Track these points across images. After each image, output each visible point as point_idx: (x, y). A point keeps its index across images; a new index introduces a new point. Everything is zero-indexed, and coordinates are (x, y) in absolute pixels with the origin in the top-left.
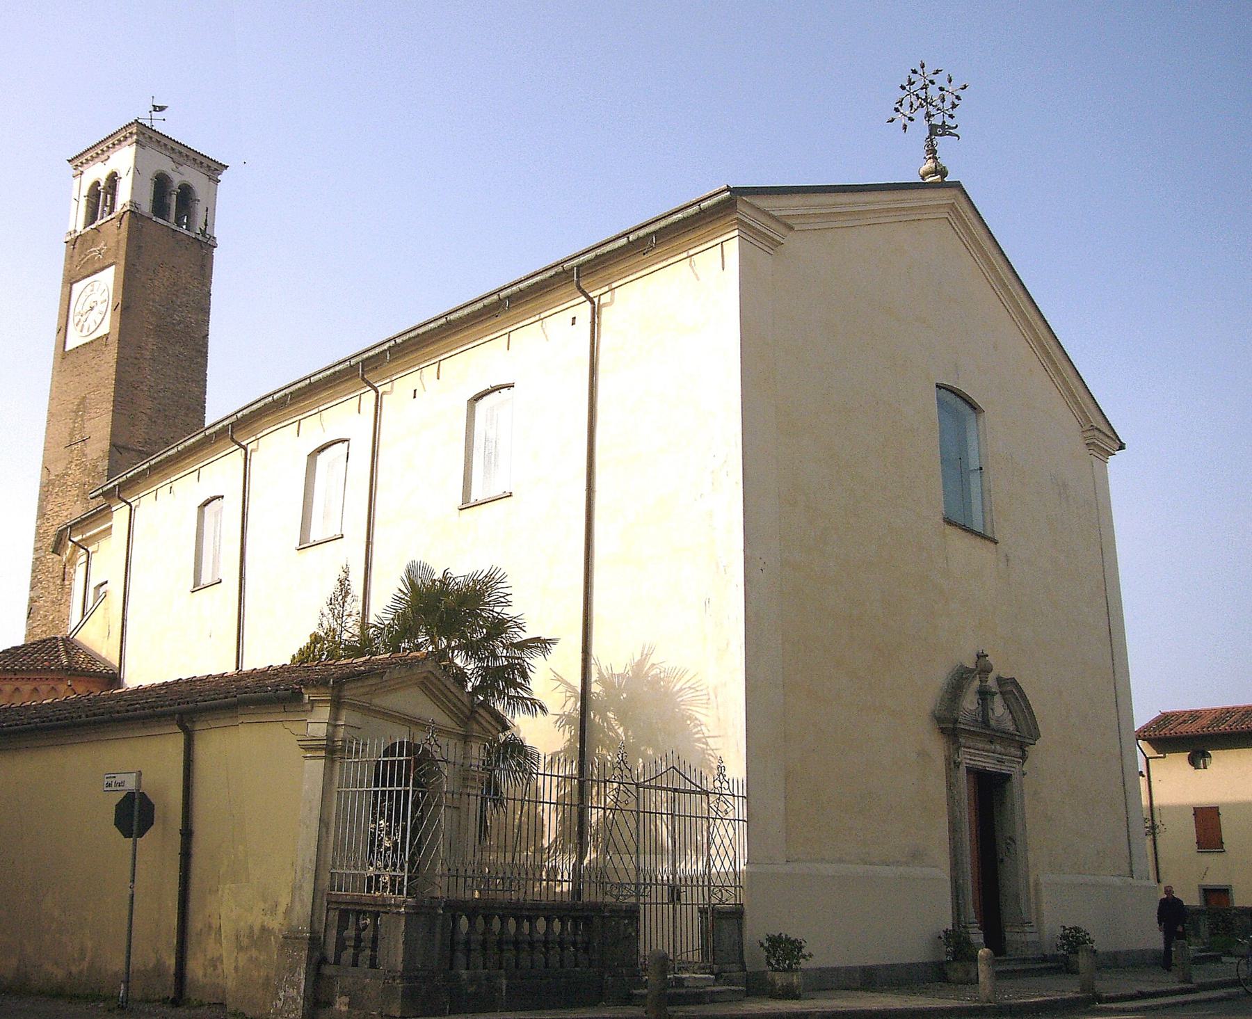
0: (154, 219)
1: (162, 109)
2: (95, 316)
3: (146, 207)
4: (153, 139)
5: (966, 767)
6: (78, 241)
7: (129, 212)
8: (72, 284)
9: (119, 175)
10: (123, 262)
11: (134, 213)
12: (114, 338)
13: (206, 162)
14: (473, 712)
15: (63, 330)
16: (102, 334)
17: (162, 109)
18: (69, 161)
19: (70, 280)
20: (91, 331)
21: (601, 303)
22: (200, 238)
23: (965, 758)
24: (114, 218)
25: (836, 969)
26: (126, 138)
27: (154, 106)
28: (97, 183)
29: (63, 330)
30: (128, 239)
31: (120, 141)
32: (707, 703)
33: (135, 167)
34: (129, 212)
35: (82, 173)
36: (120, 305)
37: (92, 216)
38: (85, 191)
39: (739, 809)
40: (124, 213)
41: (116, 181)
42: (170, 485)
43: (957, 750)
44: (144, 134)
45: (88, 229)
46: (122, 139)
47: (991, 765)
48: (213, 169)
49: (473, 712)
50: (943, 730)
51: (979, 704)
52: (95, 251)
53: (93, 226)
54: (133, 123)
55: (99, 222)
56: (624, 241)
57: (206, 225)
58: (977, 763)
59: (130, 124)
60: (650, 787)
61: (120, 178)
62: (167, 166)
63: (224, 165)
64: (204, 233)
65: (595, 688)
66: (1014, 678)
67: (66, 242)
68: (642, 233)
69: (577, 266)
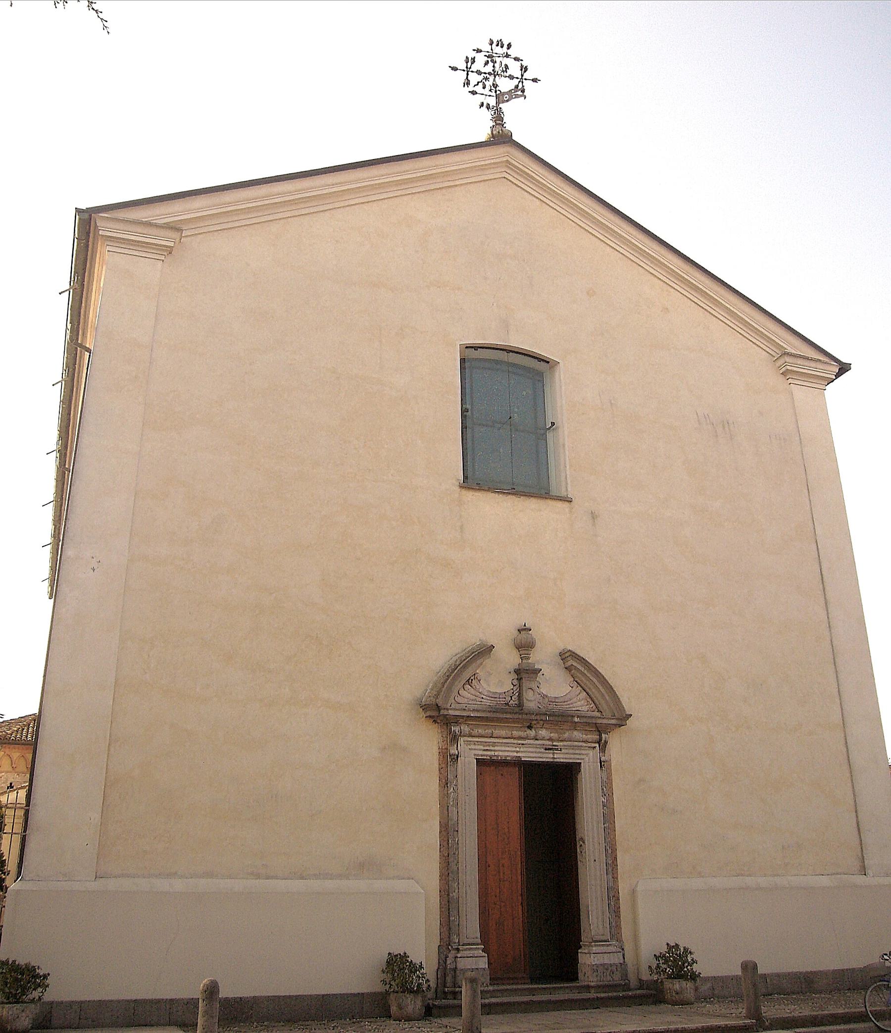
47: (531, 753)
50: (434, 719)
51: (514, 686)
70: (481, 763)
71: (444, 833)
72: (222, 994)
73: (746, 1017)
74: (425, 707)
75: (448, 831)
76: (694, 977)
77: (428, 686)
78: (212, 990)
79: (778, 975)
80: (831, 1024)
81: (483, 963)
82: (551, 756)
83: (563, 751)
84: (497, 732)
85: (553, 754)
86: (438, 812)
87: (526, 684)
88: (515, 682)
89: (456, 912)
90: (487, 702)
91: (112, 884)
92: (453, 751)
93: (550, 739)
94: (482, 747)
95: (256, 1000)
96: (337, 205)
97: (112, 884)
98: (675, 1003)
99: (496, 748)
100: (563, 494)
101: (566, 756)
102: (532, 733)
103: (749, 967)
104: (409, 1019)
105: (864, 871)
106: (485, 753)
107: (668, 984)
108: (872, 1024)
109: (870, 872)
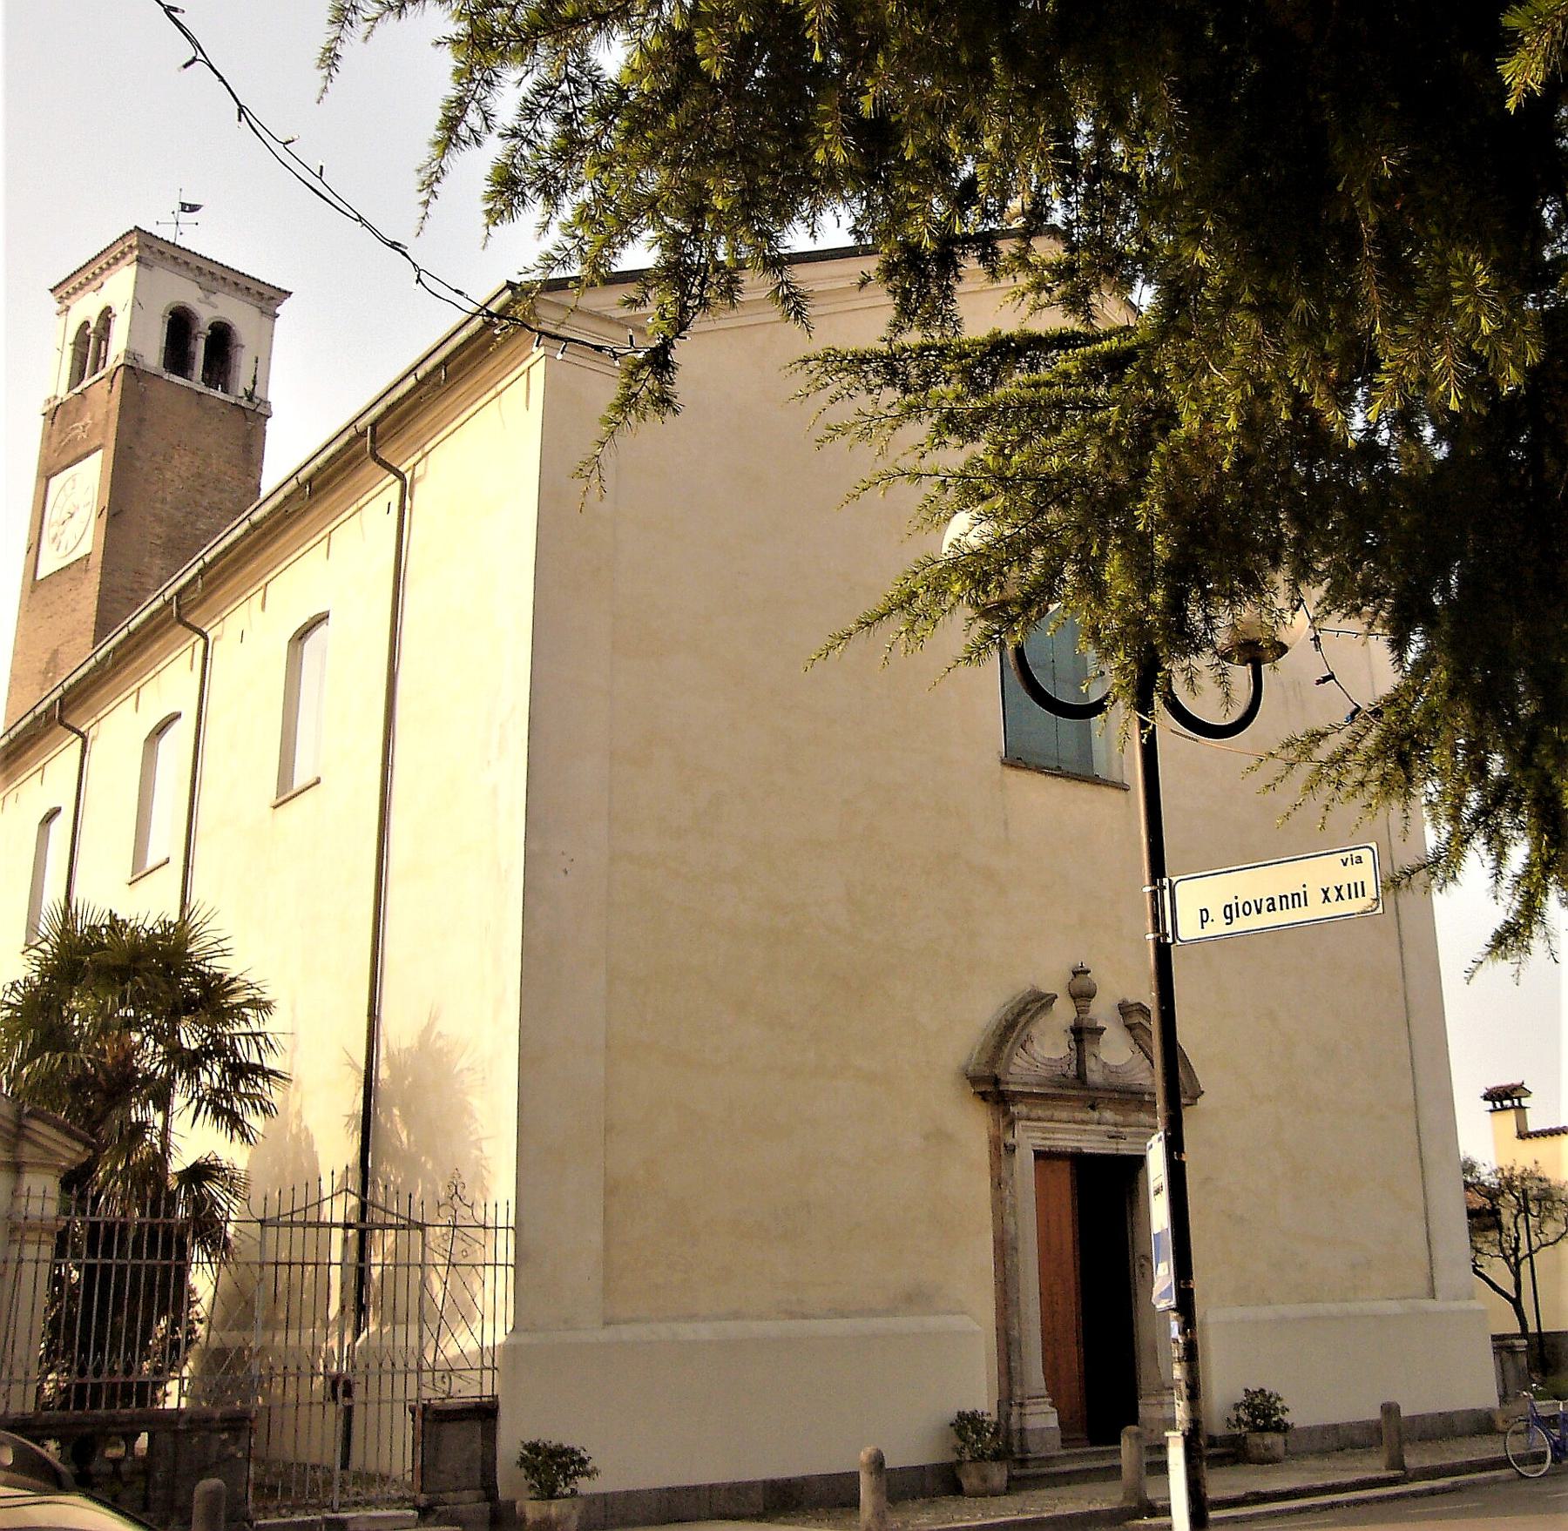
0: (166, 376)
1: (194, 208)
2: (75, 527)
3: (153, 358)
4: (167, 255)
5: (1034, 1151)
6: (59, 412)
7: (122, 368)
8: (48, 479)
9: (113, 312)
10: (112, 445)
11: (132, 370)
12: (97, 559)
13: (254, 287)
14: (20, 1126)
15: (34, 549)
16: (82, 554)
17: (194, 208)
18: (52, 290)
19: (47, 474)
20: (69, 549)
21: (416, 476)
22: (244, 403)
23: (1028, 1138)
24: (103, 378)
25: (712, 1487)
26: (124, 254)
27: (182, 203)
28: (86, 324)
29: (34, 549)
30: (121, 407)
31: (116, 260)
32: (483, 1085)
33: (135, 297)
34: (122, 368)
35: (68, 309)
36: (106, 510)
37: (78, 374)
38: (71, 337)
39: (505, 1247)
40: (118, 368)
41: (110, 320)
42: (15, 791)
43: (1011, 1124)
44: (150, 247)
45: (71, 395)
46: (119, 255)
47: (1093, 1142)
48: (268, 298)
49: (20, 1126)
50: (984, 1096)
51: (1071, 1049)
52: (77, 428)
53: (77, 390)
54: (131, 231)
55: (85, 383)
56: (411, 381)
57: (254, 383)
58: (1056, 1143)
59: (127, 233)
60: (292, 1224)
61: (115, 316)
62: (187, 293)
63: (286, 292)
64: (250, 396)
65: (383, 1073)
66: (1140, 1004)
67: (44, 414)
68: (429, 365)
69: (371, 425)
70: (1039, 1155)
71: (998, 1251)
72: (887, 1466)
73: (1388, 1469)
74: (974, 1080)
75: (1004, 1248)
76: (1282, 1428)
77: (973, 1049)
78: (878, 1462)
79: (1350, 1425)
80: (1469, 1472)
81: (1053, 1421)
82: (1114, 1146)
83: (1128, 1139)
84: (1058, 1114)
85: (1117, 1143)
86: (990, 1222)
87: (1088, 1048)
88: (1073, 1045)
89: (1016, 1357)
90: (1043, 1072)
91: (627, 1333)
92: (1010, 1140)
93: (1116, 1125)
94: (1039, 1134)
95: (806, 1480)
96: (840, 307)
97: (627, 1333)
98: (1262, 1461)
99: (1059, 1136)
100: (1116, 777)
101: (1134, 1147)
102: (1095, 1115)
103: (1390, 1410)
104: (995, 1494)
105: (1432, 1294)
106: (1044, 1142)
107: (1254, 1439)
108: (1511, 1471)
109: (1438, 1295)
